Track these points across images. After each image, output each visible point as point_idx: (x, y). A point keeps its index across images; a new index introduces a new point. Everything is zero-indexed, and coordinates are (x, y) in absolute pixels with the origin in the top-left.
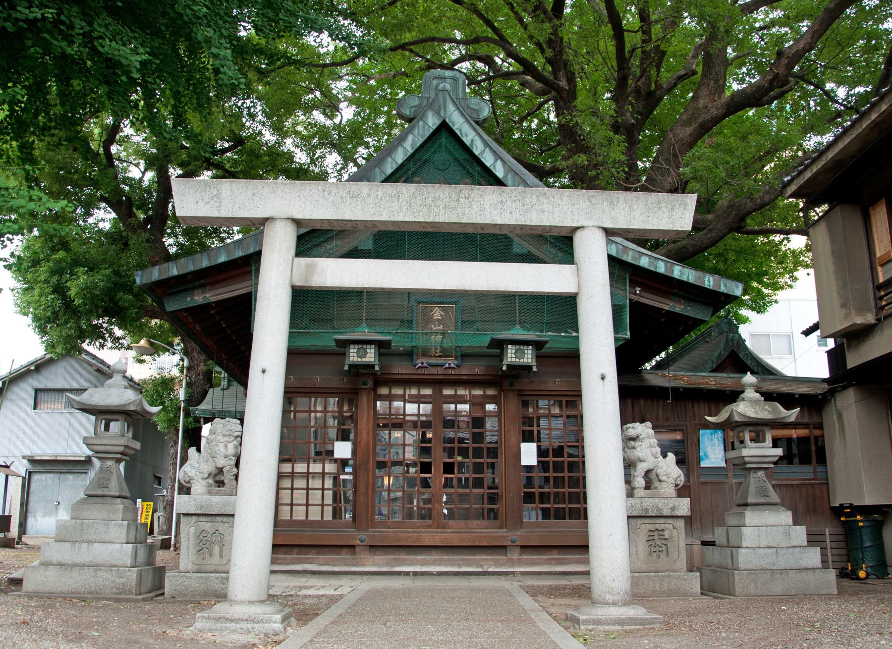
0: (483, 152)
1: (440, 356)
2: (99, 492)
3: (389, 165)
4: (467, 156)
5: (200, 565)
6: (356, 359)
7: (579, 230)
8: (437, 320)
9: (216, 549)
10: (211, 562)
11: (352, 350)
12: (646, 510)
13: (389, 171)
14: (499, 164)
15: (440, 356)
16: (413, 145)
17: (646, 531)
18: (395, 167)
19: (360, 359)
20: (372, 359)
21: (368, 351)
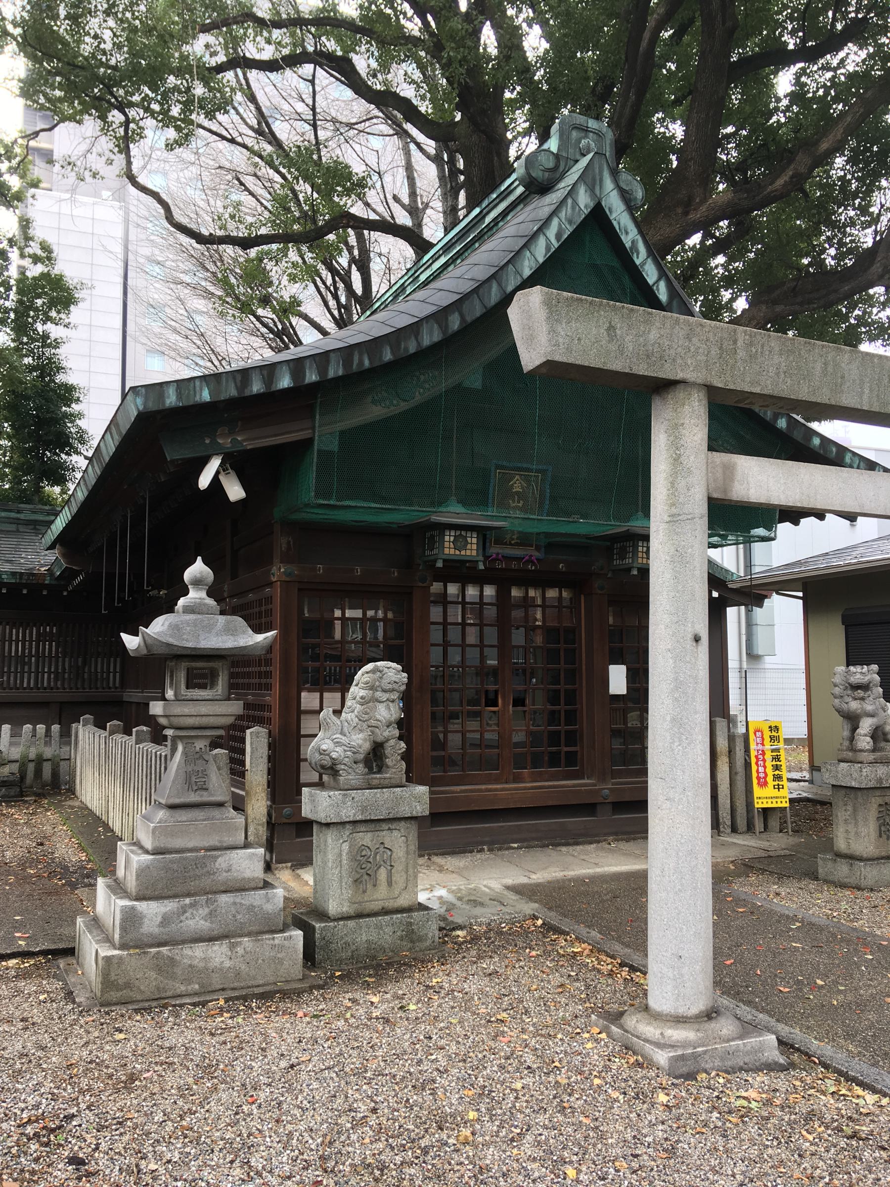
0: (643, 263)
1: (517, 544)
2: (193, 798)
3: (526, 263)
4: (615, 263)
5: (360, 903)
6: (452, 551)
7: (682, 386)
8: (517, 493)
9: (382, 874)
10: (377, 896)
11: (447, 538)
12: (880, 780)
13: (527, 272)
14: (662, 285)
15: (517, 544)
16: (558, 236)
17: (876, 806)
18: (535, 266)
19: (457, 552)
20: (474, 553)
21: (469, 539)
